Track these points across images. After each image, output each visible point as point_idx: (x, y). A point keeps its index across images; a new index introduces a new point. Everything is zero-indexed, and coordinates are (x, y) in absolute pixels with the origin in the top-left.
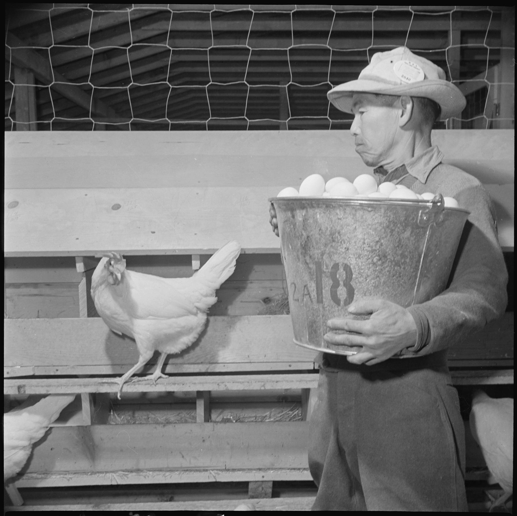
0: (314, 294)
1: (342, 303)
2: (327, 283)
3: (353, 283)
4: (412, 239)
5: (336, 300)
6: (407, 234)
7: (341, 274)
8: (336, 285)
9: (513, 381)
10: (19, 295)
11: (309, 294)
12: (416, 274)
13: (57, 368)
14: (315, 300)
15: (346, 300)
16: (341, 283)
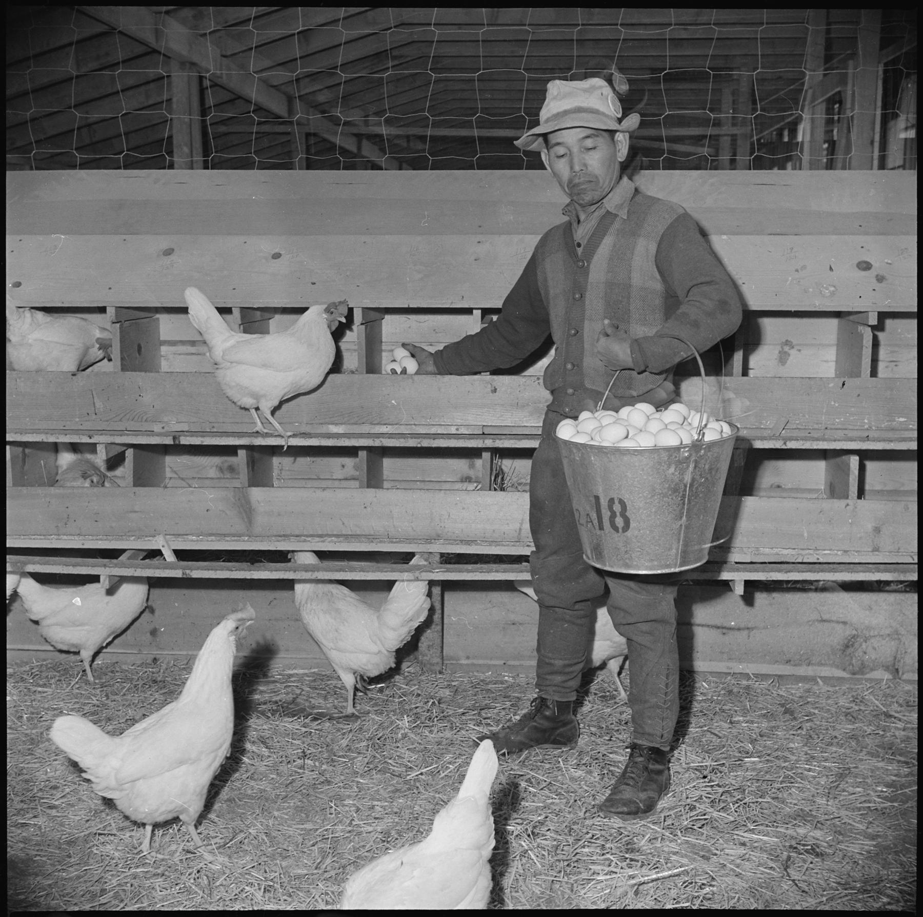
0: (596, 522)
1: (620, 530)
2: (606, 514)
3: (627, 514)
4: (677, 473)
5: (616, 529)
6: (672, 470)
7: (617, 508)
8: (613, 515)
9: (916, 484)
10: (175, 354)
11: (592, 522)
12: (684, 501)
13: (214, 424)
14: (597, 527)
15: (623, 528)
16: (618, 514)
